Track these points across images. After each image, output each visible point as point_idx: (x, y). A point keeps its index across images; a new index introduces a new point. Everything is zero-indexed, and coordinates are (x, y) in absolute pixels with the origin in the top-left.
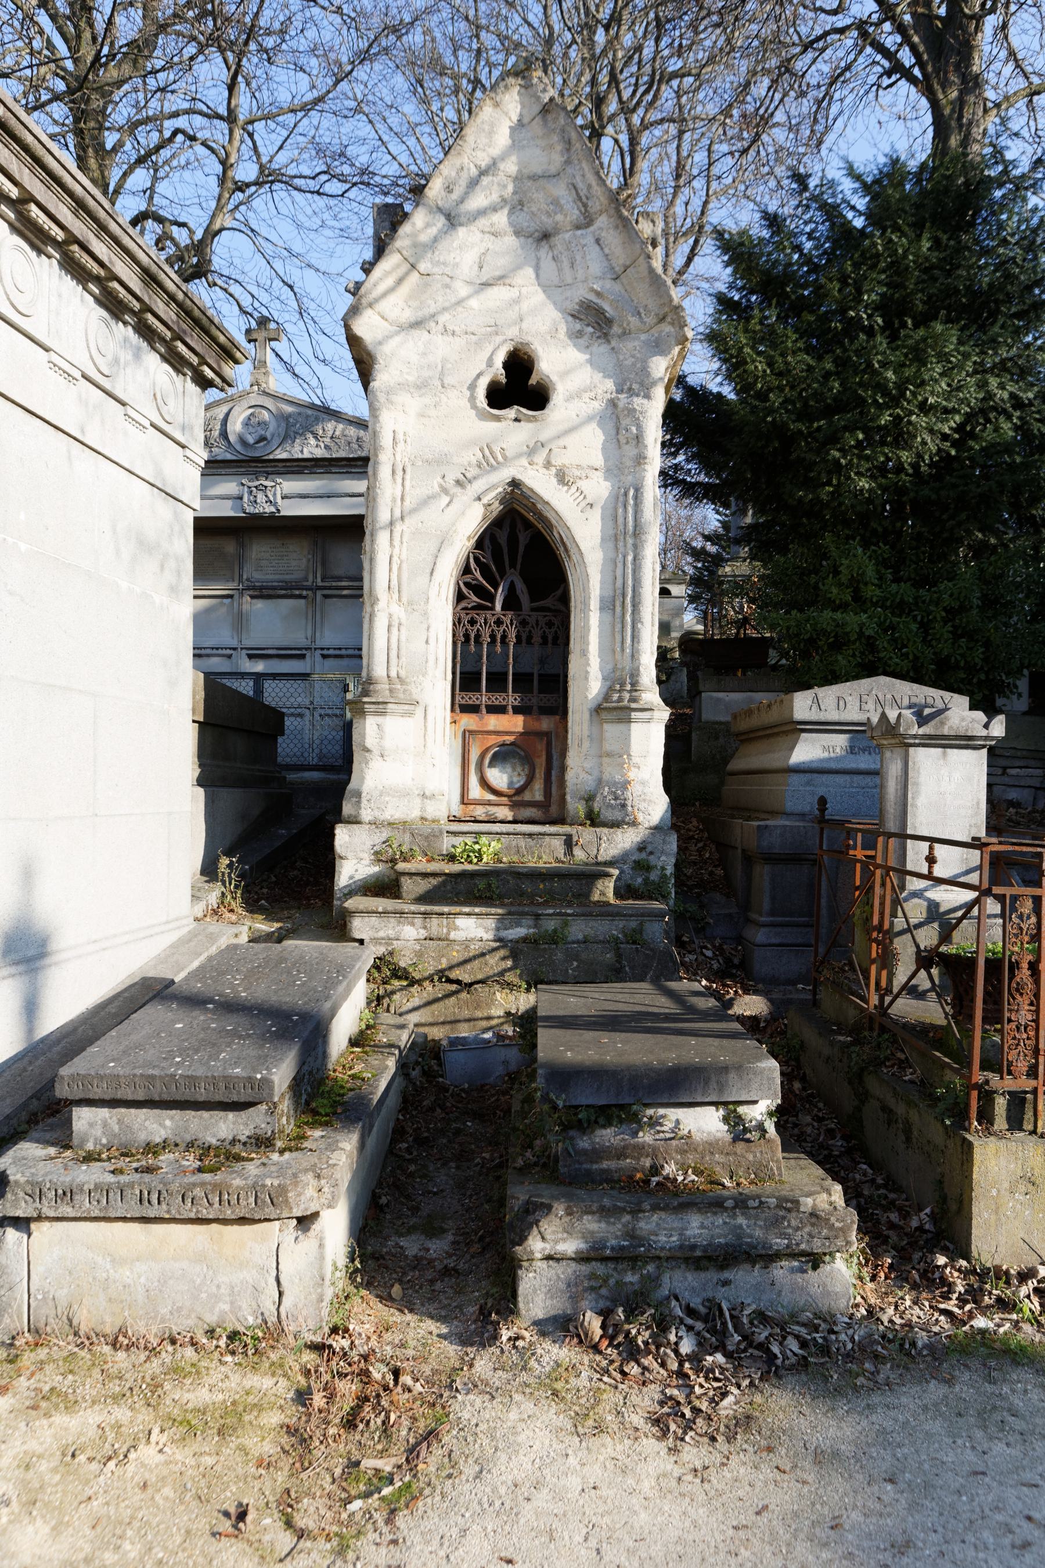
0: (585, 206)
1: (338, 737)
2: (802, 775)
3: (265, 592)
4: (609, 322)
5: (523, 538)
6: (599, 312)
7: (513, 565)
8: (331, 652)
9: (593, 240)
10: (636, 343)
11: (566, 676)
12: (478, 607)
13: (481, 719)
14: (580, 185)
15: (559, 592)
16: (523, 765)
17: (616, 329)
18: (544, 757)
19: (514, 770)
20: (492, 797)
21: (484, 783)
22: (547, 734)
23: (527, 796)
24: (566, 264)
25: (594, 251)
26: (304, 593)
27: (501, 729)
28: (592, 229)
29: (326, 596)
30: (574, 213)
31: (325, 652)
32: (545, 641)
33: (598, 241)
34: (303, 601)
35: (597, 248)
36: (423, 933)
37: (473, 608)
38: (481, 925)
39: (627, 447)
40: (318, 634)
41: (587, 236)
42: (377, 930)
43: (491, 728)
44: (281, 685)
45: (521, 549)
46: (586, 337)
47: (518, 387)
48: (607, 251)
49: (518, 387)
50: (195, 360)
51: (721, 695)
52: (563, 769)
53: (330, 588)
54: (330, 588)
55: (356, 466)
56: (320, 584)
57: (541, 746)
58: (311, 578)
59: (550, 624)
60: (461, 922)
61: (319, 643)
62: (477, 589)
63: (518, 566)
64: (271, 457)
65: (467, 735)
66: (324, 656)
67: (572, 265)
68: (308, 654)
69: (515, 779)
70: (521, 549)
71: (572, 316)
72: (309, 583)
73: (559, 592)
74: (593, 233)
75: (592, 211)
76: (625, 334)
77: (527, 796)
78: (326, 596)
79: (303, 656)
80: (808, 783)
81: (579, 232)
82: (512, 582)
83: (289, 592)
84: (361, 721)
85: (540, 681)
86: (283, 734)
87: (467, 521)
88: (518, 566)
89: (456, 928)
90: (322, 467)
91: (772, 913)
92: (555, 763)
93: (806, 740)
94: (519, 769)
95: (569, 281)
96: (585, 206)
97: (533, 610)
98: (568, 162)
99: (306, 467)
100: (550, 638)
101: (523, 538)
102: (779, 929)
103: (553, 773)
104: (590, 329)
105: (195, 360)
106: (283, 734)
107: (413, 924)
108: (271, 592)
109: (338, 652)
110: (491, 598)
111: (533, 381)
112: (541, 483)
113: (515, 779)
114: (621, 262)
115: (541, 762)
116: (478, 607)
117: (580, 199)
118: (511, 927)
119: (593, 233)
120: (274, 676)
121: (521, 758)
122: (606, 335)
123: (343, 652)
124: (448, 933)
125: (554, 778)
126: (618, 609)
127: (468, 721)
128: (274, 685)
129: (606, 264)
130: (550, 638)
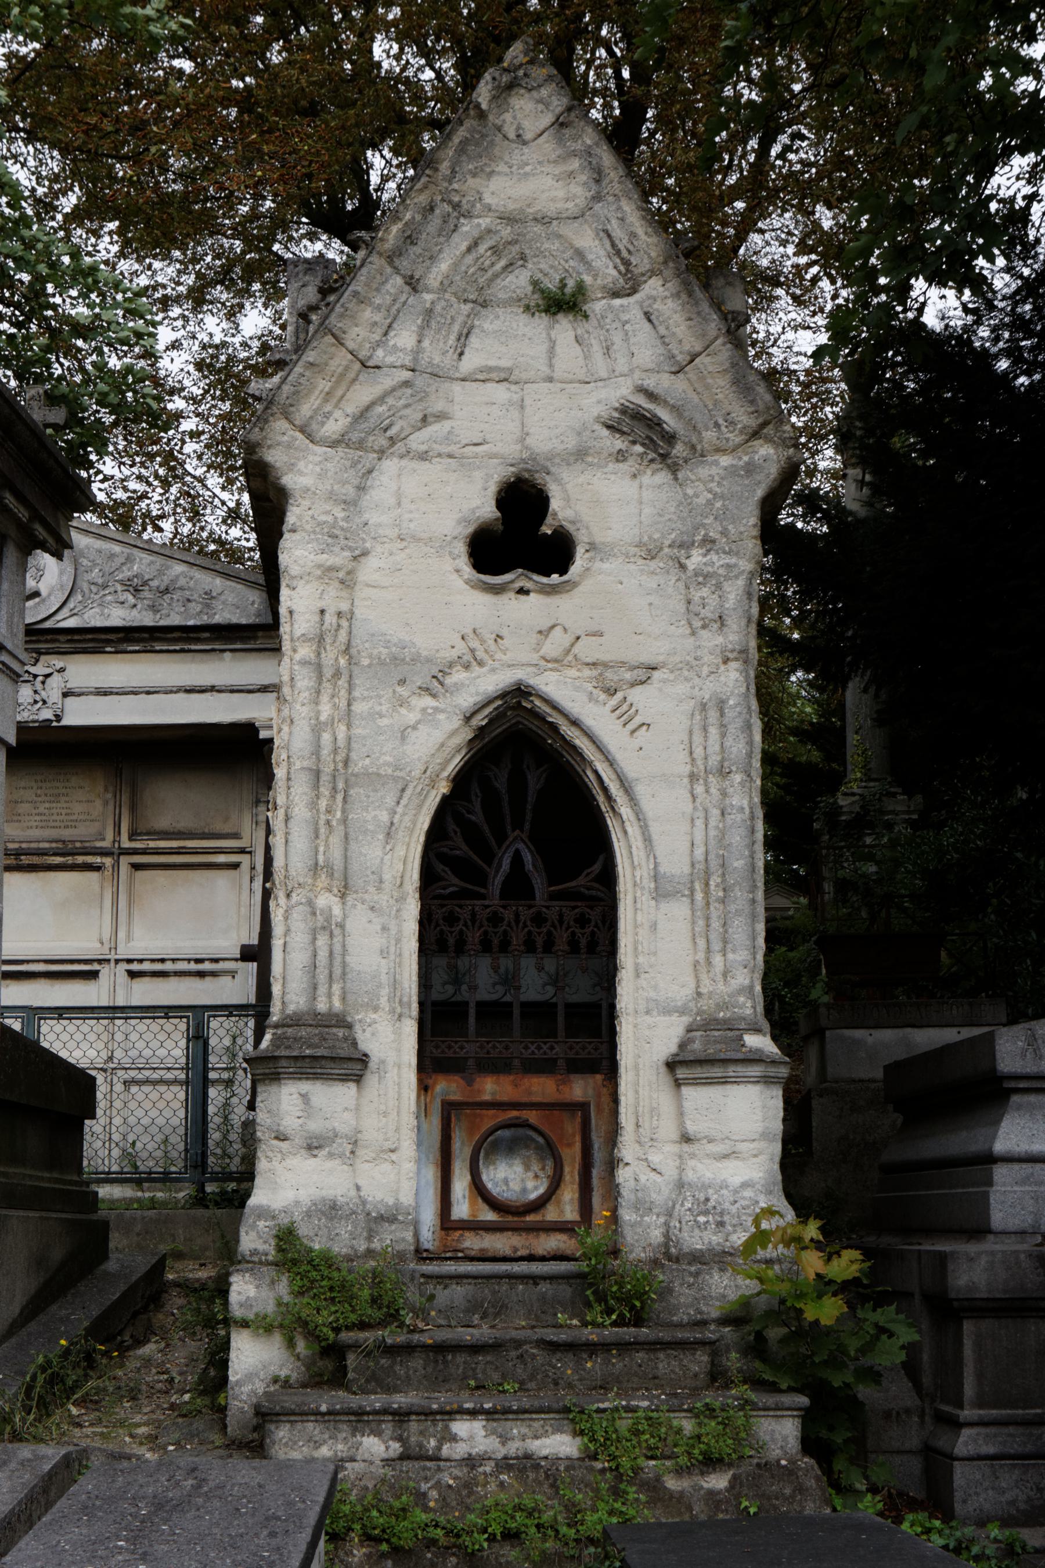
0: (627, 263)
1: (175, 1122)
2: (1016, 1166)
3: (25, 860)
4: (671, 438)
5: (534, 781)
6: (653, 423)
7: (518, 825)
8: (146, 966)
9: (640, 315)
10: (714, 471)
11: (612, 1007)
12: (463, 894)
13: (470, 1083)
14: (617, 233)
15: (597, 867)
16: (542, 1159)
17: (679, 450)
18: (578, 1147)
19: (527, 1168)
20: (489, 1216)
21: (478, 1188)
22: (583, 1107)
23: (551, 1214)
24: (597, 349)
25: (643, 331)
26: (98, 860)
27: (505, 1098)
28: (637, 297)
29: (136, 867)
30: (609, 272)
31: (135, 967)
32: (574, 947)
33: (648, 316)
34: (94, 876)
35: (647, 325)
36: (396, 1447)
37: (452, 896)
38: (494, 1432)
39: (704, 634)
40: (122, 935)
41: (631, 306)
42: (318, 1445)
43: (487, 1097)
44: (71, 1028)
45: (531, 798)
46: (631, 461)
47: (520, 539)
48: (662, 330)
49: (520, 539)
50: (23, 514)
51: (858, 1034)
52: (612, 1164)
53: (144, 852)
54: (144, 852)
55: (198, 640)
56: (126, 844)
57: (572, 1127)
58: (110, 835)
59: (582, 921)
60: (461, 1427)
61: (123, 952)
62: (460, 866)
63: (527, 826)
64: (47, 625)
65: (449, 1111)
66: (133, 975)
67: (607, 351)
68: (105, 971)
69: (530, 1184)
70: (531, 798)
71: (609, 427)
72: (106, 844)
73: (597, 867)
74: (641, 304)
75: (636, 271)
76: (697, 453)
77: (551, 1214)
78: (136, 867)
79: (93, 975)
80: (1025, 1181)
81: (617, 302)
82: (517, 852)
83: (70, 860)
84: (273, 1089)
85: (523, 1015)
86: (93, 1116)
87: (423, 744)
88: (527, 826)
89: (454, 1439)
90: (137, 641)
91: (981, 1403)
92: (598, 1155)
93: (1019, 1107)
94: (536, 1167)
95: (604, 374)
96: (627, 263)
97: (552, 897)
98: (598, 198)
99: (108, 642)
100: (583, 942)
101: (534, 781)
102: (992, 1430)
103: (595, 1172)
104: (638, 449)
105: (23, 514)
106: (93, 1116)
107: (378, 1434)
108: (36, 860)
109: (158, 967)
110: (482, 880)
111: (547, 530)
112: (565, 691)
113: (530, 1184)
114: (687, 347)
115: (572, 1156)
116: (463, 894)
117: (618, 253)
118: (546, 1434)
119: (641, 304)
120: (61, 1013)
121: (538, 1148)
122: (664, 457)
123: (168, 966)
124: (439, 1448)
125: (595, 1182)
126: (699, 896)
127: (446, 1087)
128: (58, 1028)
129: (661, 350)
130: (583, 942)
